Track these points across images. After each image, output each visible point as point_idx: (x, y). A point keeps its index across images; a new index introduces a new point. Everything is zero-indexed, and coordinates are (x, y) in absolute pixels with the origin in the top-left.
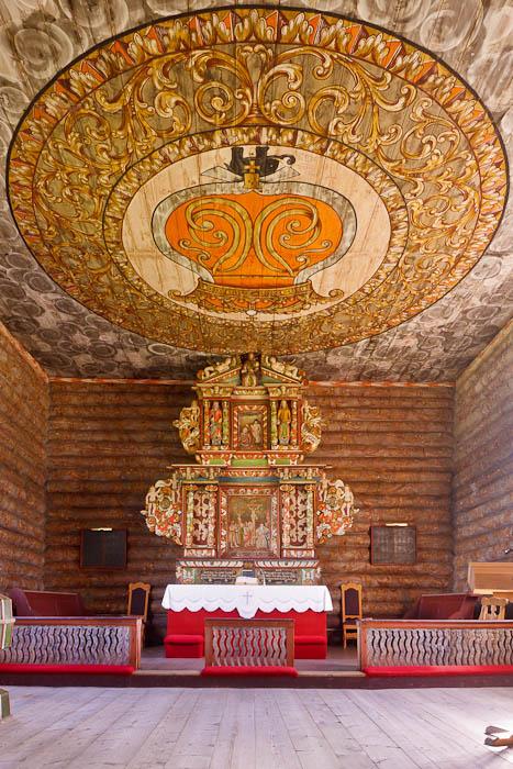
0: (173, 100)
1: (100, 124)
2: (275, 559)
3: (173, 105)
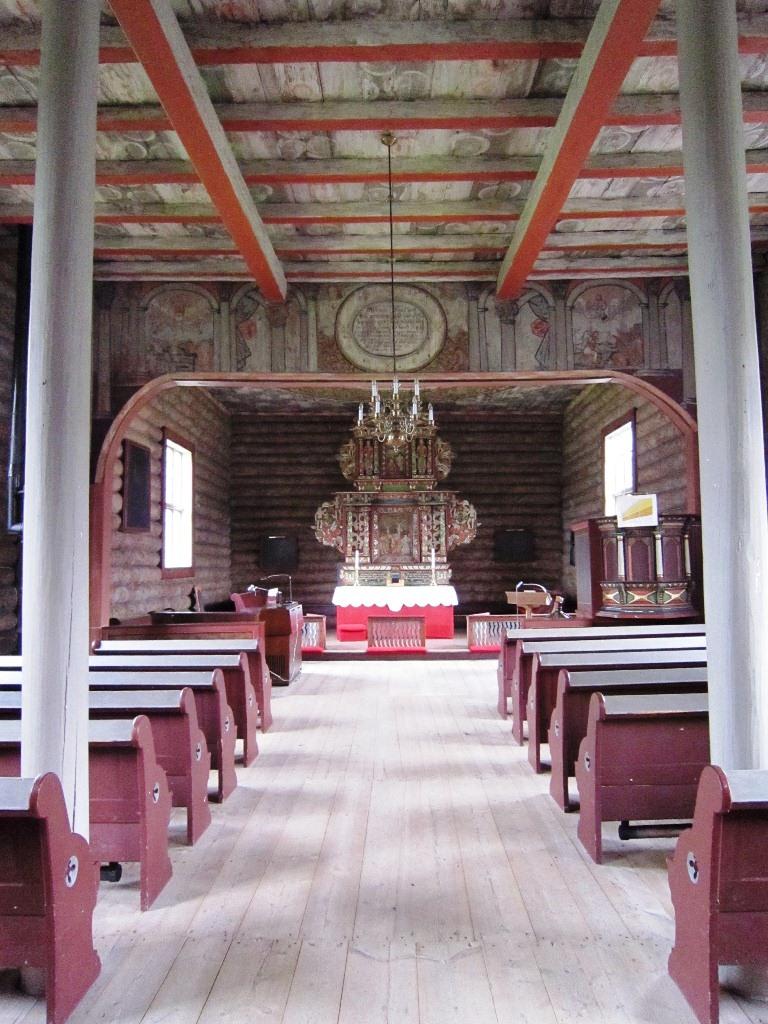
2: (416, 563)
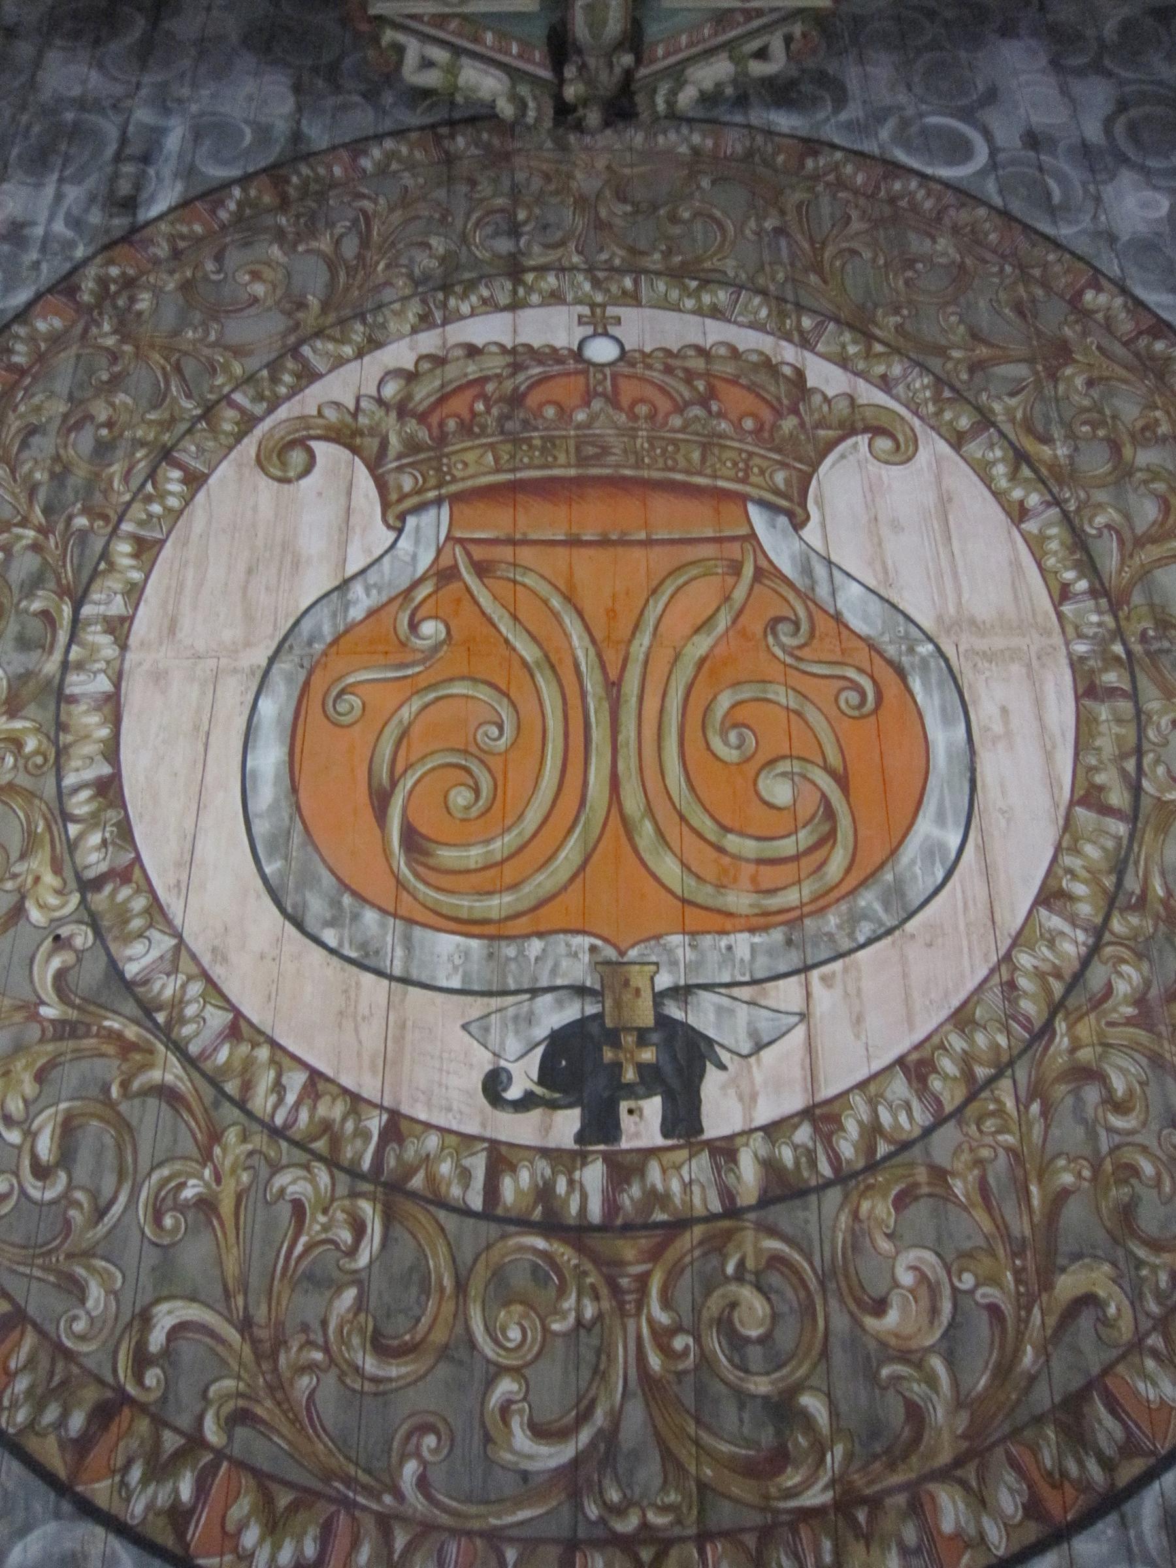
0: (892, 1318)
1: (1127, 1213)
3: (895, 1299)
